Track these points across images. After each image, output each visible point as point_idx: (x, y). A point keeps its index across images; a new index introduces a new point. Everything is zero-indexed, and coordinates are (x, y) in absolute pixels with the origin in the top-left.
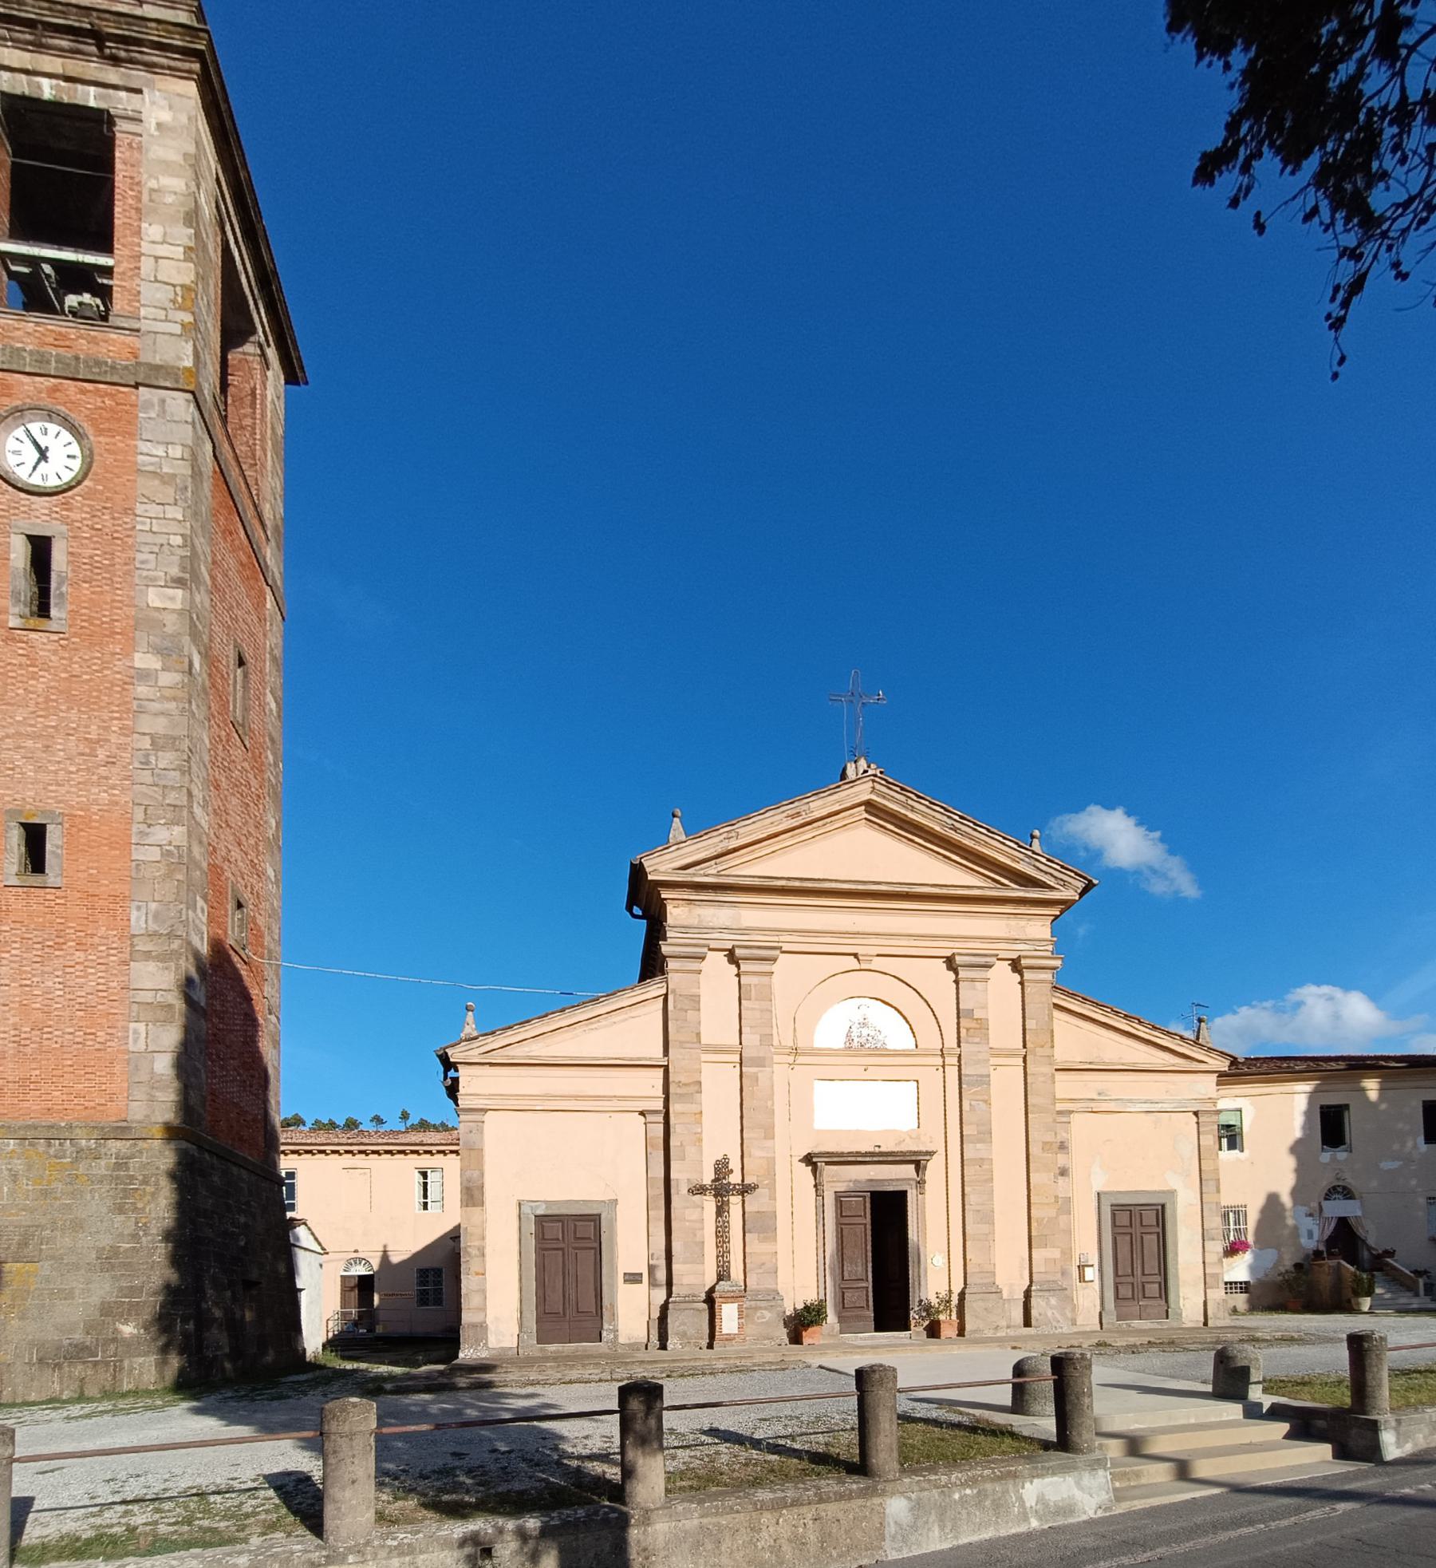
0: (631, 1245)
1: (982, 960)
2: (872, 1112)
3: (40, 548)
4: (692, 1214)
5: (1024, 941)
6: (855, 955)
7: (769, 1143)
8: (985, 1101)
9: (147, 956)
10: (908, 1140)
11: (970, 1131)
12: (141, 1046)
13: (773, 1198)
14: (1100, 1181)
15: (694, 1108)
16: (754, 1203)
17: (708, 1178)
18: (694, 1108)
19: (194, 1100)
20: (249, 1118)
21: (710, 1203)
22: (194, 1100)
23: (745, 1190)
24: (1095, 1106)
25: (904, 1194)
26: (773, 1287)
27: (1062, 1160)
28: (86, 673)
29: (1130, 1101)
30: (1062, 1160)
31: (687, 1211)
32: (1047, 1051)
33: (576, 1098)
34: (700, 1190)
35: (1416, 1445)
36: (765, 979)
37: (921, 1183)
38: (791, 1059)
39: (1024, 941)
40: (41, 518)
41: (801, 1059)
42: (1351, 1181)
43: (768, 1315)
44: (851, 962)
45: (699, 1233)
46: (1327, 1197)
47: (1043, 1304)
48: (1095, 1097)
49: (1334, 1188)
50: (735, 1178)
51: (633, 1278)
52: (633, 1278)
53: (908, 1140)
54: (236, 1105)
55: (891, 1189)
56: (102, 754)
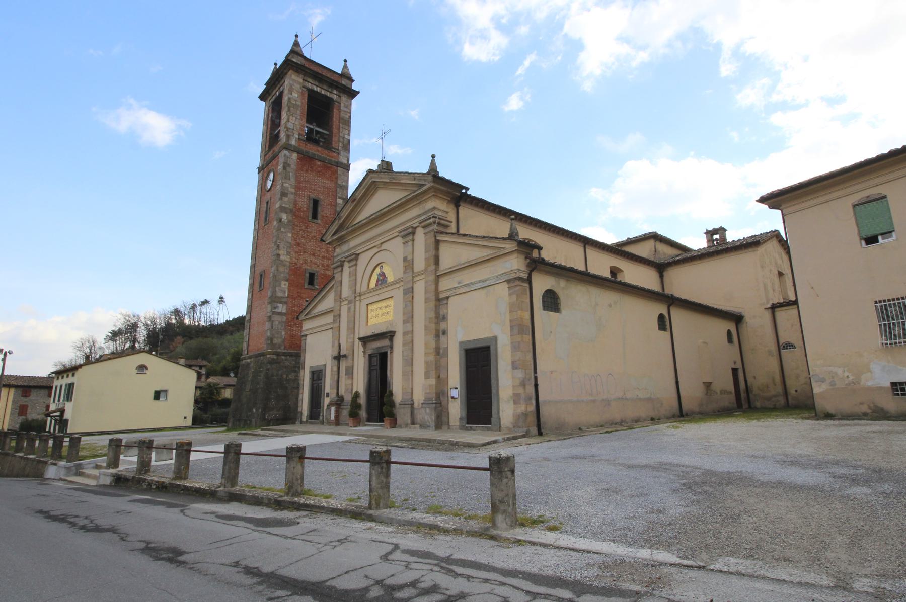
28: (270, 353)
29: (472, 283)
37: (391, 347)
48: (457, 285)
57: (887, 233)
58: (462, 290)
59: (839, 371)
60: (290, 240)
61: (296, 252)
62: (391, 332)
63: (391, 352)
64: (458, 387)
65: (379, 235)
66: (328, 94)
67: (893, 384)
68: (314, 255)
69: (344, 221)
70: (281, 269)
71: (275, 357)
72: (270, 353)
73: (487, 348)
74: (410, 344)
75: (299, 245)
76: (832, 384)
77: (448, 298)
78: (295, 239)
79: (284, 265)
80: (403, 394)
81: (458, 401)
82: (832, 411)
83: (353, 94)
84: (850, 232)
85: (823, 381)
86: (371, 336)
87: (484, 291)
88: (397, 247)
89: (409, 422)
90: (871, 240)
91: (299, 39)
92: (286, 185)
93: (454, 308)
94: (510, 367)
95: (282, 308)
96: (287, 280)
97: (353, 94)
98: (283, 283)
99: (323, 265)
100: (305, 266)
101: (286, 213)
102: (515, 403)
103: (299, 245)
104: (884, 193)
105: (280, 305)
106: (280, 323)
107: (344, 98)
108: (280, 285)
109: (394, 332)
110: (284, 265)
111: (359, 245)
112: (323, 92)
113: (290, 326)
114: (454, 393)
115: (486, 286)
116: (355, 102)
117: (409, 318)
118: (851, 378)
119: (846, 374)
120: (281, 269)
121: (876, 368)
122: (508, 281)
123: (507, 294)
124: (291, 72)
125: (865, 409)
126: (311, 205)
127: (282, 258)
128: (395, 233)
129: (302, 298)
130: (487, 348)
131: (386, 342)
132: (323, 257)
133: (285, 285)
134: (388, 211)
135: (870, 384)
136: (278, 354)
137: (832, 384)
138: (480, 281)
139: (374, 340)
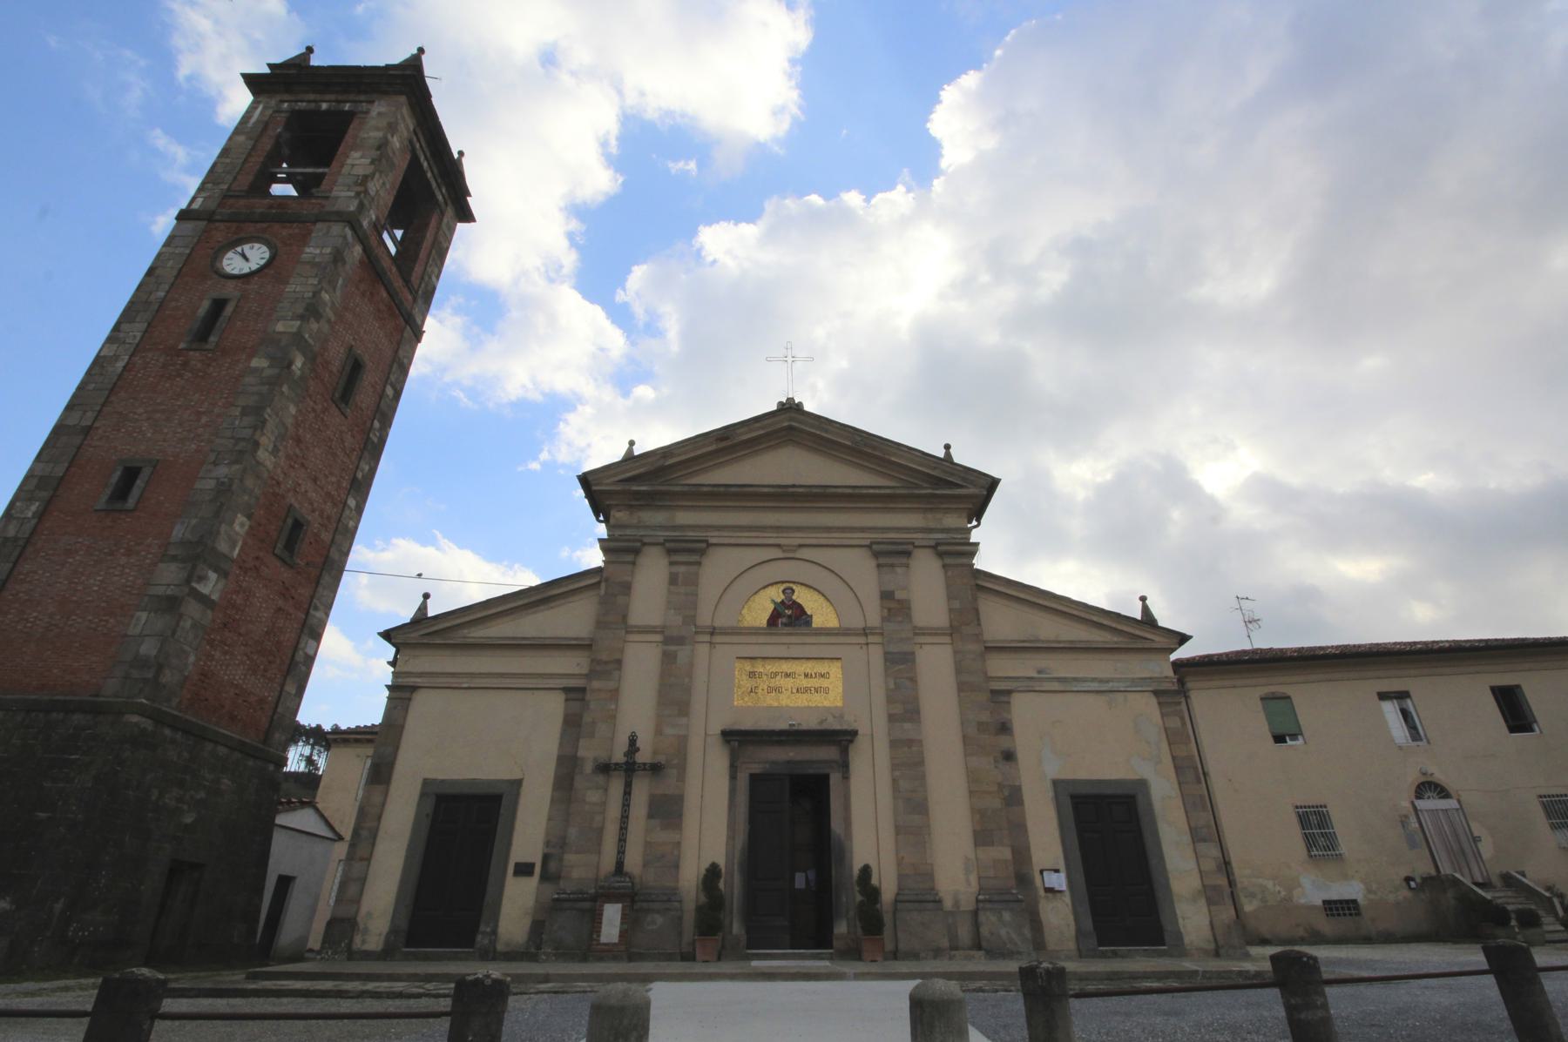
0: (528, 835)
1: (900, 548)
2: (807, 690)
4: (593, 797)
7: (684, 720)
10: (830, 719)
11: (904, 709)
14: (1055, 769)
17: (619, 756)
19: (219, 169)
22: (219, 169)
23: (655, 769)
25: (826, 778)
27: (1003, 742)
28: (141, 711)
29: (1075, 679)
30: (1003, 742)
33: (502, 675)
34: (605, 768)
36: (693, 569)
37: (845, 766)
40: (230, 290)
41: (718, 639)
42: (1439, 776)
43: (659, 920)
44: (778, 553)
46: (1419, 795)
47: (993, 919)
49: (1423, 784)
50: (643, 757)
51: (524, 870)
52: (524, 870)
55: (811, 771)
56: (204, 419)
57: (1294, 737)
59: (1270, 884)
60: (289, 421)
61: (288, 457)
63: (846, 777)
64: (1062, 865)
66: (434, 185)
67: (1325, 902)
68: (315, 480)
69: (671, 466)
70: (249, 482)
71: (148, 724)
72: (141, 711)
75: (298, 441)
77: (1009, 692)
78: (297, 425)
80: (901, 877)
81: (1067, 899)
82: (1268, 936)
83: (466, 215)
85: (1252, 895)
88: (860, 569)
89: (945, 943)
90: (1279, 739)
91: (424, 57)
92: (326, 296)
93: (1025, 711)
94: (1187, 838)
95: (211, 585)
96: (249, 517)
98: (240, 518)
99: (322, 512)
100: (291, 499)
101: (304, 355)
102: (1210, 902)
103: (298, 441)
105: (213, 576)
107: (450, 212)
108: (231, 523)
109: (854, 733)
112: (429, 175)
113: (211, 643)
114: (1058, 881)
115: (1105, 690)
117: (904, 709)
120: (249, 482)
121: (1306, 881)
122: (1156, 693)
124: (403, 99)
125: (1301, 932)
126: (348, 369)
127: (262, 455)
130: (1073, 797)
131: (827, 753)
132: (328, 494)
133: (240, 524)
135: (1302, 901)
136: (159, 718)
139: (780, 743)
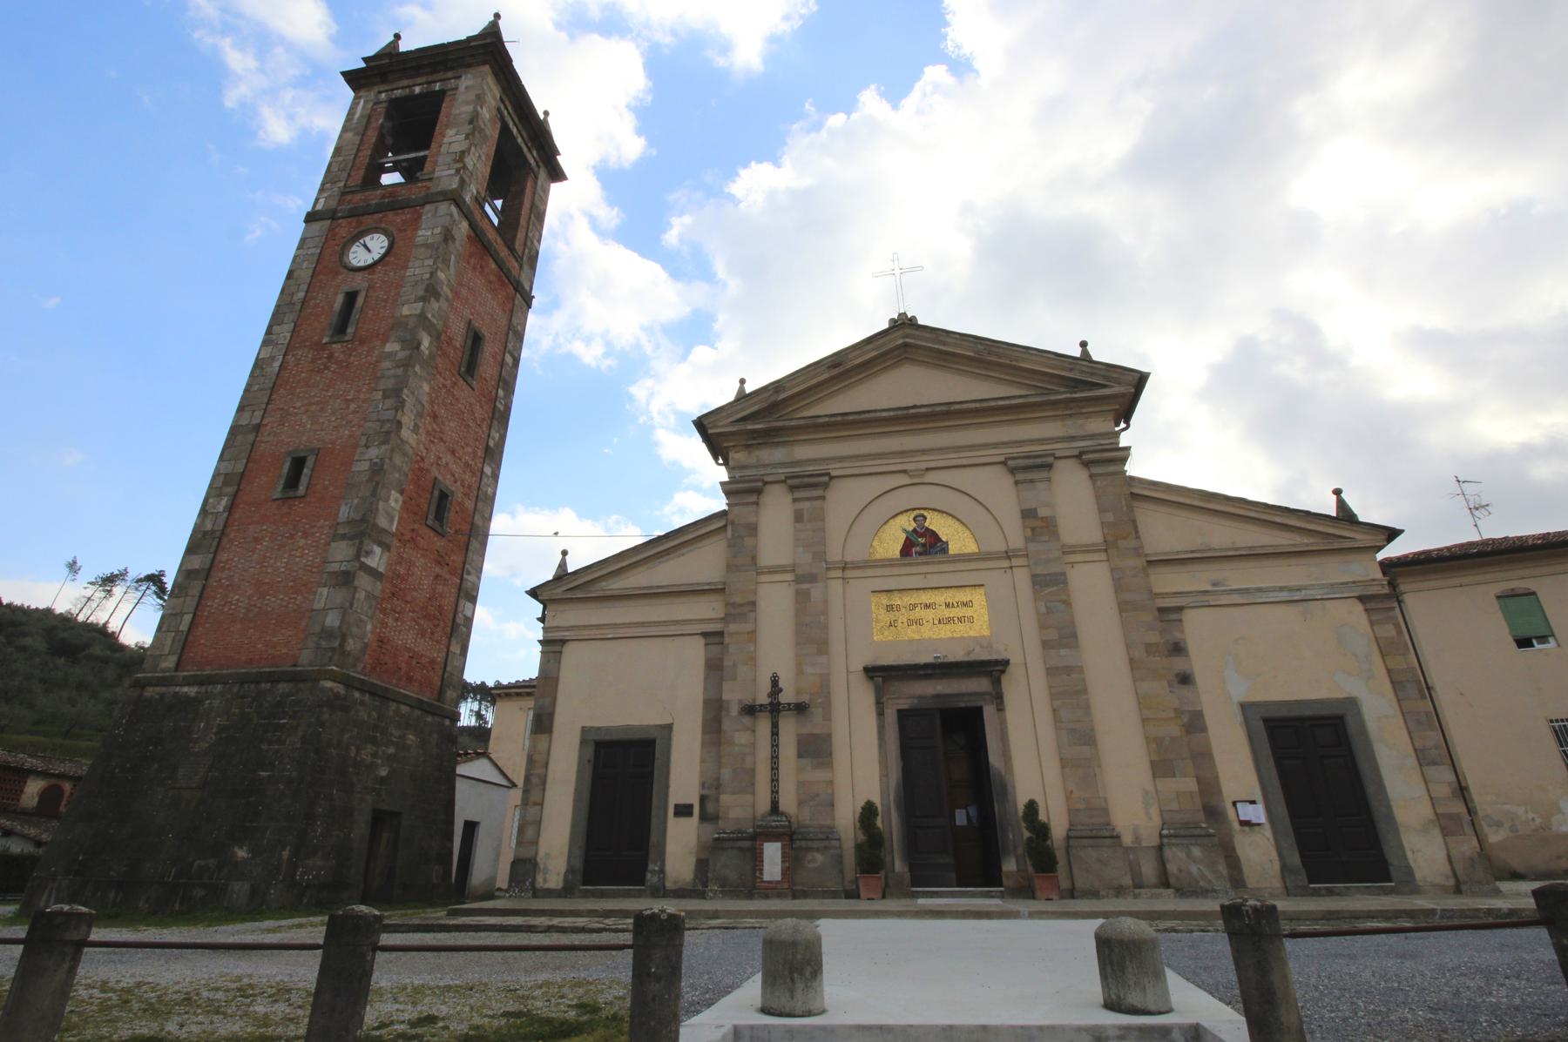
0: (684, 777)
2: (951, 620)
3: (351, 297)
4: (742, 738)
5: (1084, 438)
6: (905, 471)
7: (822, 659)
8: (1064, 602)
9: (344, 537)
10: (978, 649)
12: (322, 605)
13: (828, 716)
14: (1241, 690)
15: (747, 627)
16: (814, 725)
18: (747, 627)
20: (424, 660)
21: (764, 725)
23: (800, 709)
24: (1212, 600)
26: (828, 822)
27: (1179, 664)
28: (333, 677)
29: (1260, 590)
30: (1179, 664)
31: (737, 735)
32: (1131, 543)
34: (750, 710)
35: (380, 992)
36: (818, 503)
37: (998, 698)
38: (1006, 564)
39: (1084, 438)
40: (359, 282)
41: (849, 574)
43: (819, 858)
44: (903, 480)
45: (749, 760)
47: (1181, 854)
48: (1209, 588)
51: (684, 811)
52: (684, 811)
53: (978, 649)
54: (409, 650)
57: (1543, 639)
58: (1225, 600)
59: (1521, 811)
61: (428, 433)
62: (997, 662)
63: (1001, 708)
64: (1258, 796)
65: (923, 452)
66: (525, 150)
68: (453, 452)
69: (784, 400)
71: (340, 689)
73: (1267, 721)
74: (1069, 688)
76: (1513, 829)
77: (1180, 609)
78: (432, 402)
79: (405, 454)
84: (1498, 631)
85: (1499, 824)
86: (926, 666)
87: (1299, 607)
90: (1524, 643)
91: (500, 22)
94: (1412, 761)
97: (557, 174)
102: (1445, 832)
103: (435, 417)
104: (1533, 589)
105: (377, 550)
106: (369, 596)
107: (542, 174)
108: (387, 500)
110: (405, 454)
111: (841, 459)
113: (383, 611)
116: (555, 189)
118: (1538, 821)
119: (1530, 815)
120: (398, 460)
123: (1364, 616)
124: (487, 68)
126: (469, 342)
128: (998, 455)
129: (417, 547)
130: (1267, 721)
131: (980, 685)
132: (467, 464)
134: (925, 415)
136: (349, 683)
137: (1513, 829)
138: (1282, 589)
